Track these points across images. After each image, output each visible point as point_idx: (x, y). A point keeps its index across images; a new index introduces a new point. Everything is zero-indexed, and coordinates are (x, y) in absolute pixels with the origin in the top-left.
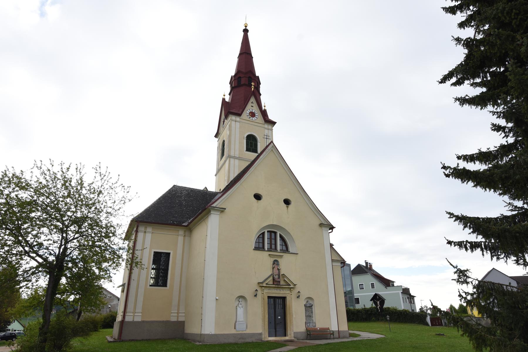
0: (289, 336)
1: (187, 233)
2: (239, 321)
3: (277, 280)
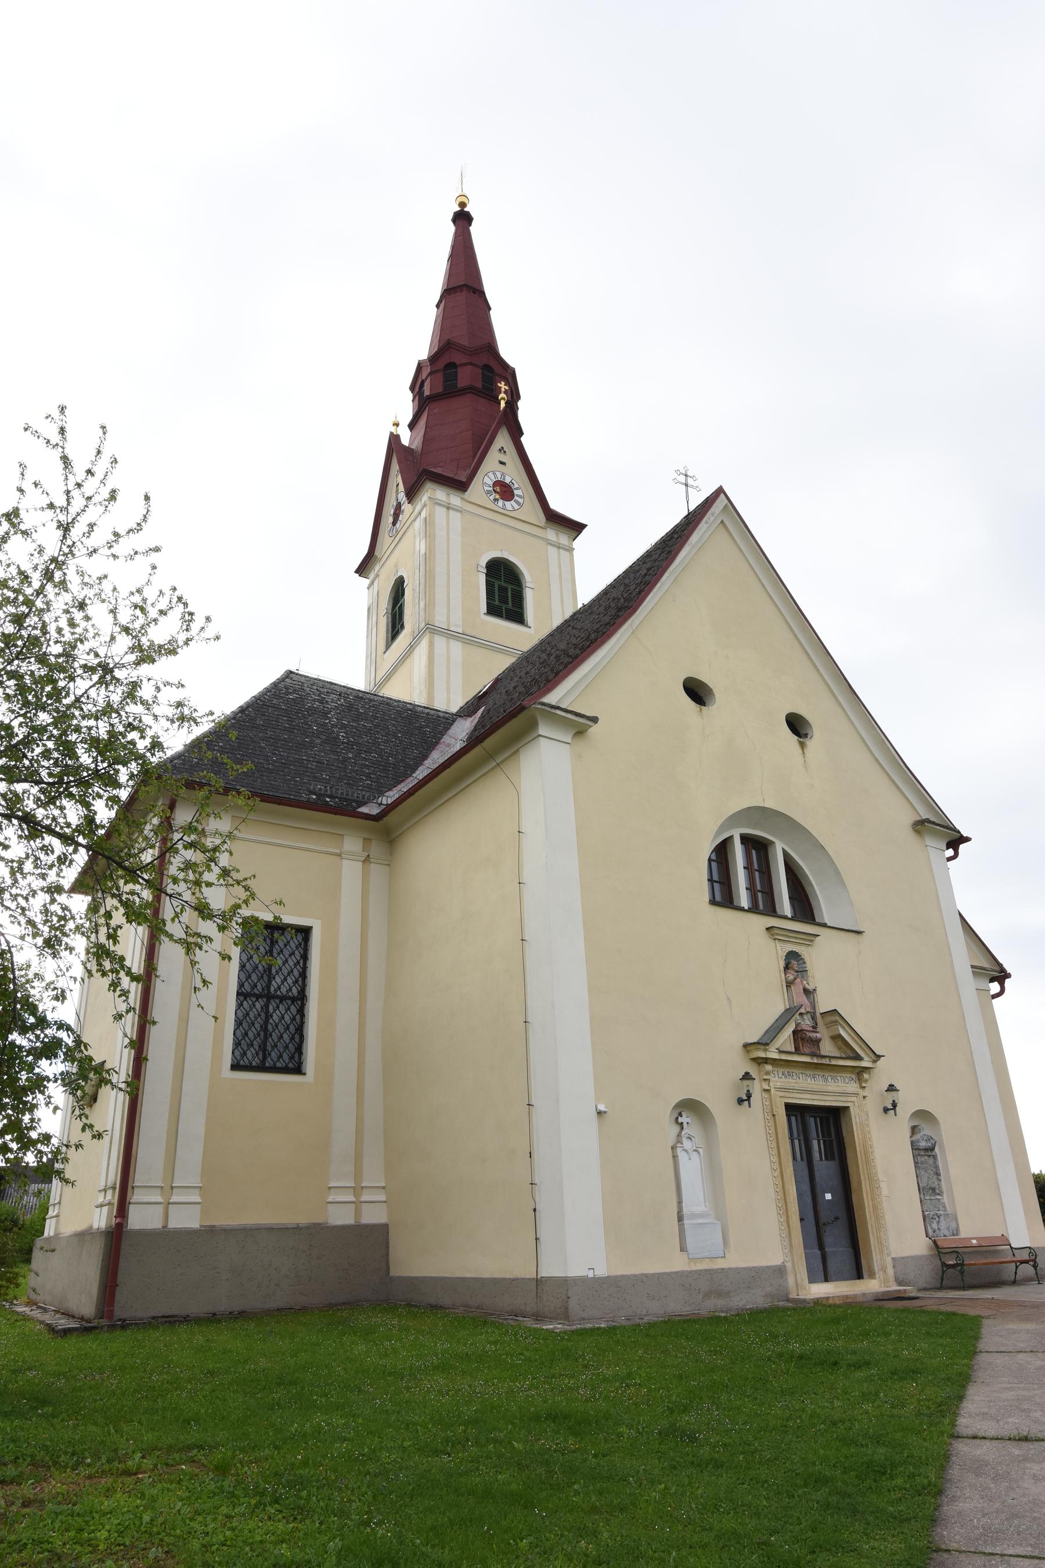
0: (879, 1274)
1: (377, 849)
2: (694, 1216)
3: (811, 1037)
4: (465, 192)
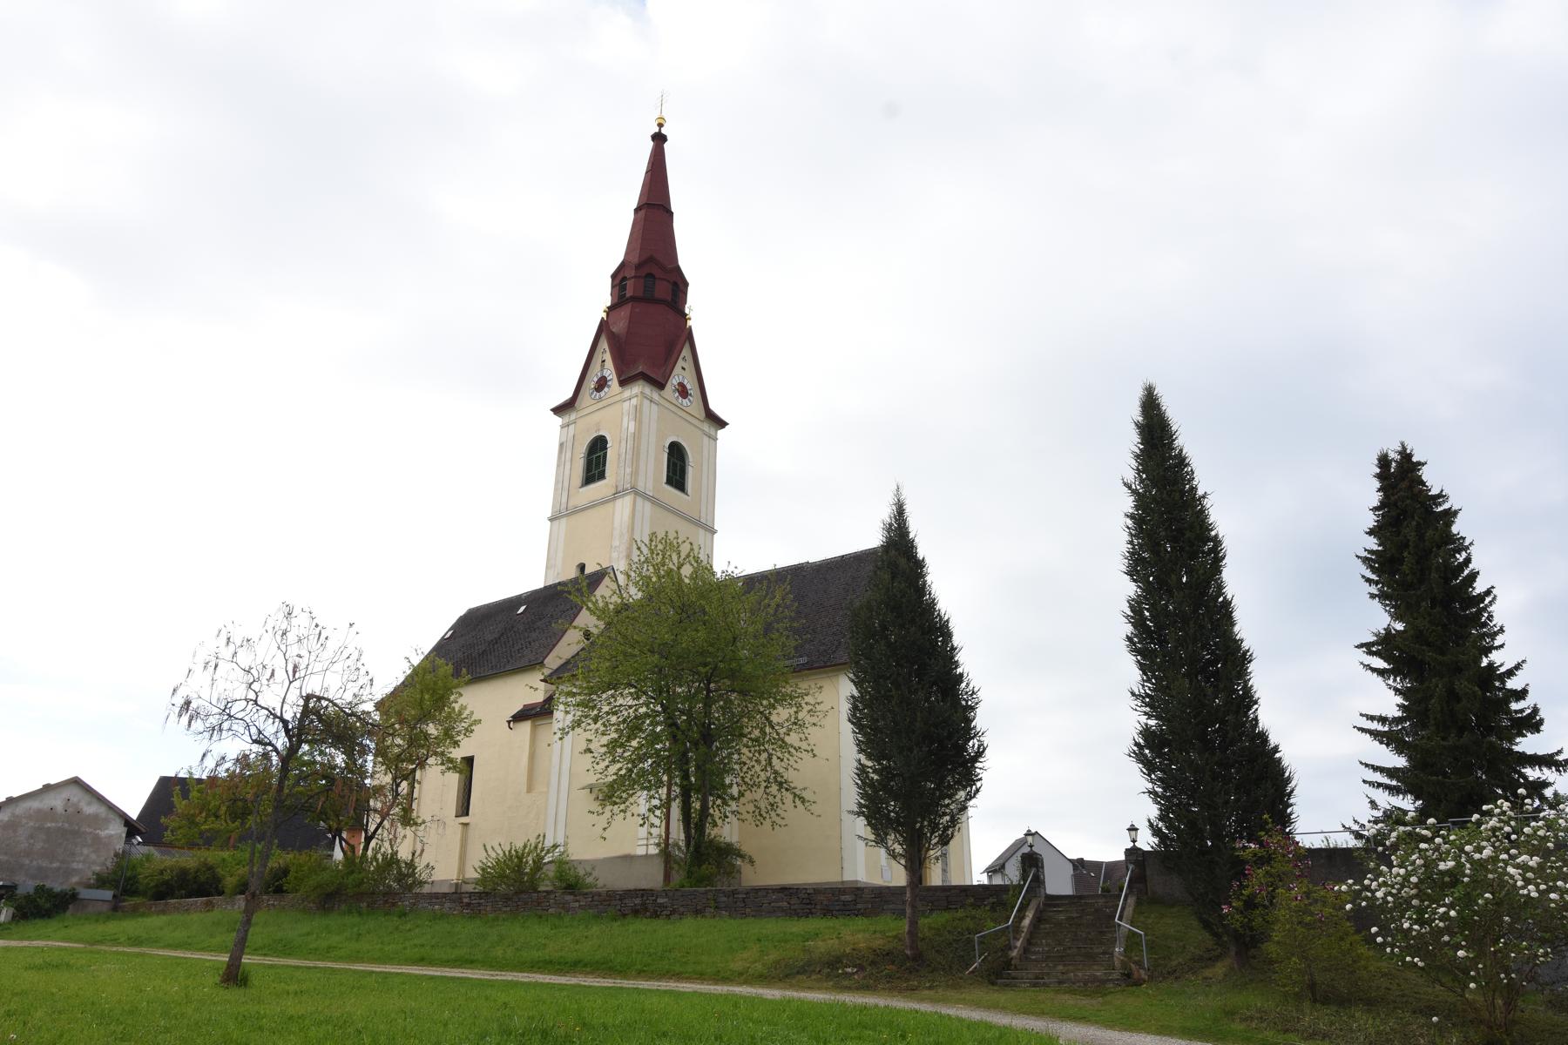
4: (664, 115)
